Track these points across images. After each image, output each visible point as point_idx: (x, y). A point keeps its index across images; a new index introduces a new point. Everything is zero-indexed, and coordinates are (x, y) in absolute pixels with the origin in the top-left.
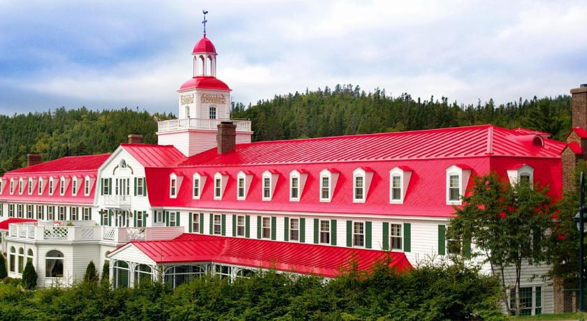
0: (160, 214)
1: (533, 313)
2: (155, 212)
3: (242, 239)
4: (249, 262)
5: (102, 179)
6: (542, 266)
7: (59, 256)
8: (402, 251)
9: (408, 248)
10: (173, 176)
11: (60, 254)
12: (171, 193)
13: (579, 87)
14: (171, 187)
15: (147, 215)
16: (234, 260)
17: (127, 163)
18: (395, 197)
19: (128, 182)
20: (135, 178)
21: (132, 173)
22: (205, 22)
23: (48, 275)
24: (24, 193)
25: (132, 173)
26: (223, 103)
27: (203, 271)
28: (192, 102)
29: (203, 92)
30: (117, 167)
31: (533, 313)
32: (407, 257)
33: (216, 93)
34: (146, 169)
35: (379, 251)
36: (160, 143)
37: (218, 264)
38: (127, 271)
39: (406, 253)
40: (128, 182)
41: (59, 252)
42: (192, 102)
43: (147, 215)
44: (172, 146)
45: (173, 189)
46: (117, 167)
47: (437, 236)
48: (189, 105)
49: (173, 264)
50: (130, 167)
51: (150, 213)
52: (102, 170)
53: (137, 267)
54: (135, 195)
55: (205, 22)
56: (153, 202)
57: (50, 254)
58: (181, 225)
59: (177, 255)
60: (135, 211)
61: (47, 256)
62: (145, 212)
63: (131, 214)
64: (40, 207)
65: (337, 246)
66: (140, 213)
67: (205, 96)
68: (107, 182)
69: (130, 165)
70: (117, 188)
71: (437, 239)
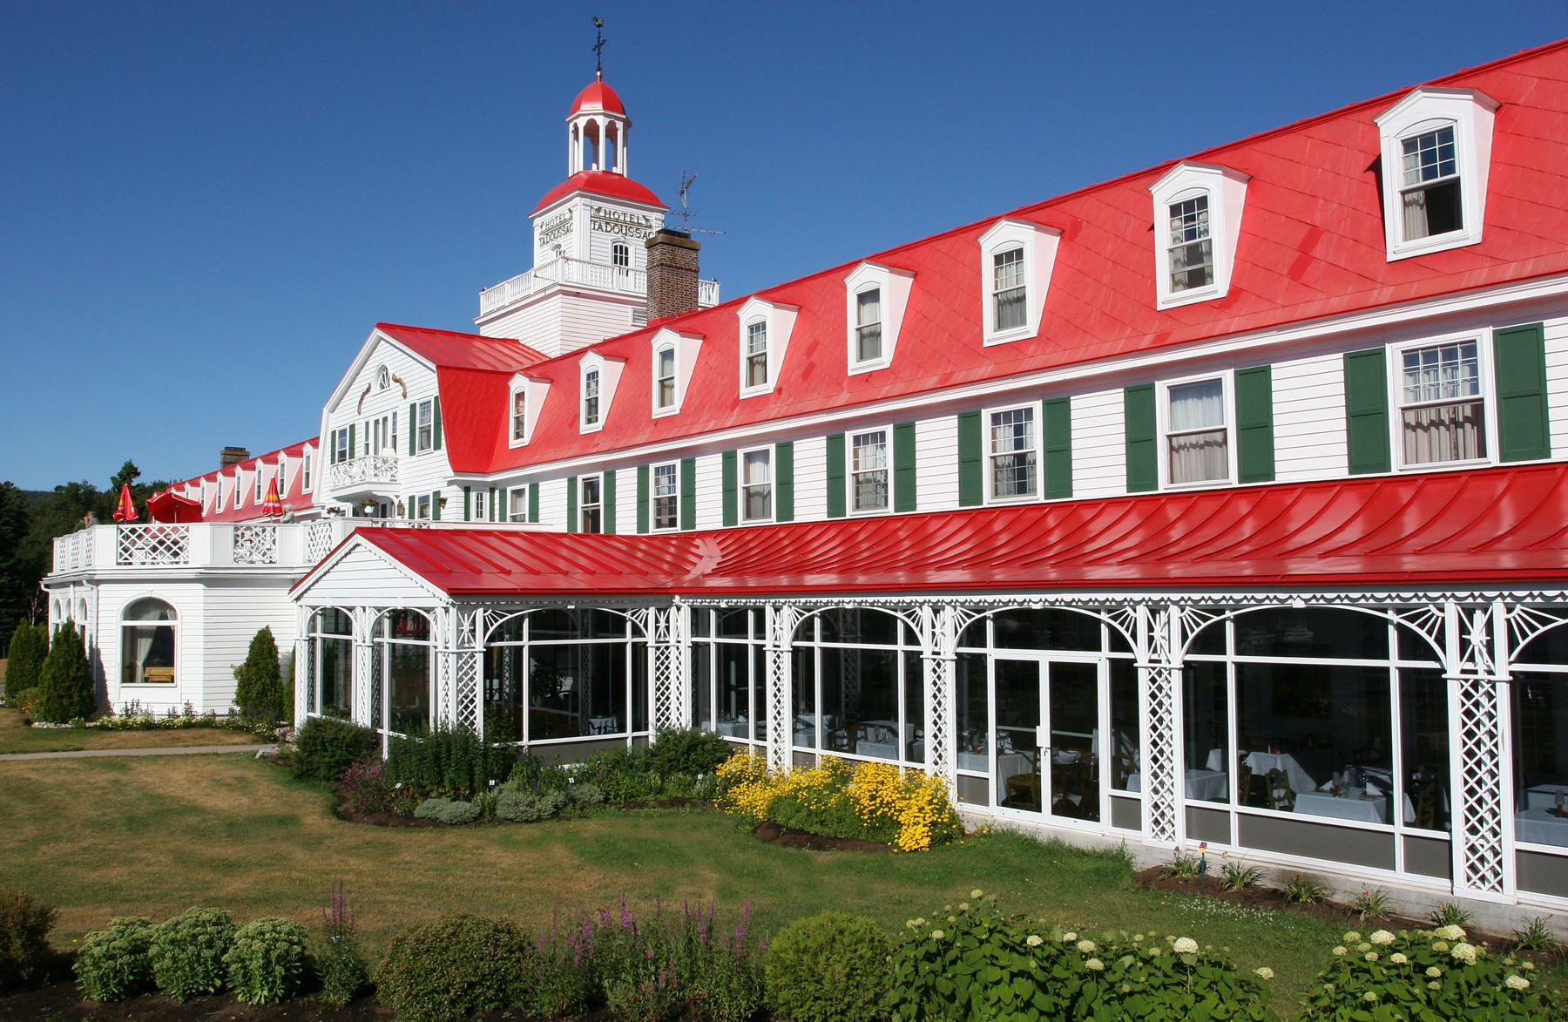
6: (229, 664)
7: (163, 617)
12: (571, 136)
14: (512, 414)
15: (444, 501)
19: (394, 423)
20: (413, 407)
21: (405, 396)
22: (598, 46)
23: (129, 675)
25: (405, 396)
27: (637, 631)
29: (597, 204)
37: (698, 602)
38: (426, 648)
40: (394, 423)
43: (444, 501)
44: (515, 342)
45: (519, 423)
46: (368, 390)
48: (561, 241)
50: (397, 381)
54: (412, 452)
55: (598, 46)
56: (458, 464)
57: (138, 609)
59: (538, 573)
62: (437, 494)
63: (401, 506)
66: (424, 500)
67: (602, 214)
69: (398, 376)
70: (367, 445)
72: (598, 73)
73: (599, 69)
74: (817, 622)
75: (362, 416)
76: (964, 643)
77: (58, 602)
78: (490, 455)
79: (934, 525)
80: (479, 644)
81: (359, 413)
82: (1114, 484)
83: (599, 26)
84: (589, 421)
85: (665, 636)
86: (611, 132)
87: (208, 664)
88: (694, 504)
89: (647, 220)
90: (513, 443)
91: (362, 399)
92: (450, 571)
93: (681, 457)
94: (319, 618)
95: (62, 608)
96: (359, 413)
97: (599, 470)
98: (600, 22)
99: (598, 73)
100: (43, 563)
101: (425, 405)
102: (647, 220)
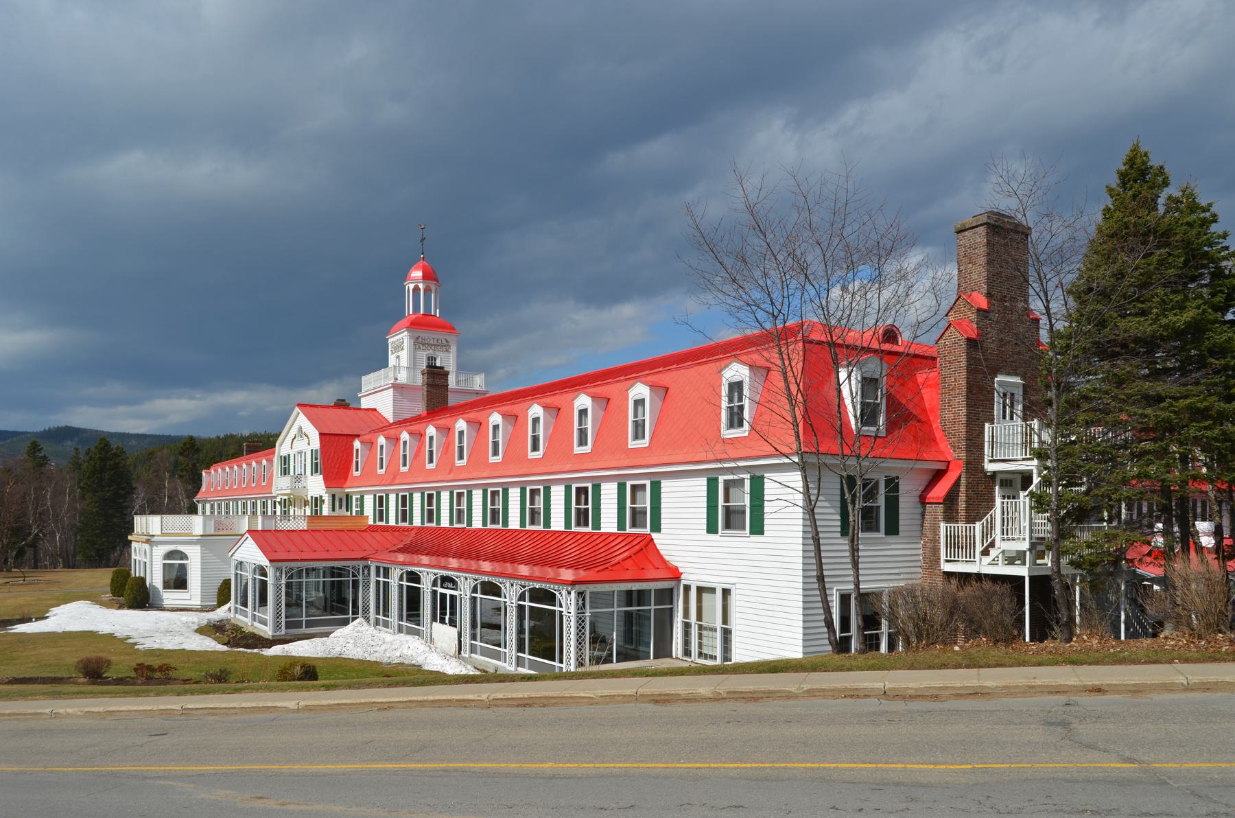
0: (341, 500)
1: (884, 647)
2: (334, 496)
3: (405, 527)
4: (550, 572)
5: (281, 456)
7: (182, 559)
8: (647, 531)
9: (656, 527)
10: (357, 444)
11: (183, 556)
13: (971, 219)
16: (425, 559)
17: (304, 430)
18: (636, 437)
20: (312, 450)
21: (309, 444)
22: (423, 240)
24: (238, 486)
25: (309, 444)
26: (447, 351)
28: (403, 349)
29: (417, 334)
30: (295, 437)
31: (884, 647)
32: (656, 541)
33: (436, 337)
34: (320, 434)
35: (611, 534)
36: (363, 407)
39: (654, 535)
41: (182, 552)
42: (403, 349)
44: (375, 410)
47: (705, 499)
48: (400, 354)
49: (299, 564)
51: (326, 497)
52: (281, 445)
53: (435, 581)
54: (312, 475)
55: (423, 240)
56: (328, 482)
57: (170, 555)
58: (365, 515)
60: (312, 497)
61: (165, 559)
64: (253, 502)
65: (552, 529)
67: (420, 340)
68: (285, 460)
71: (705, 505)
72: (422, 256)
73: (423, 254)
74: (479, 587)
75: (293, 450)
76: (554, 603)
77: (135, 548)
78: (346, 478)
79: (612, 538)
80: (283, 581)
81: (292, 448)
82: (309, 514)
83: (422, 229)
84: (636, 437)
85: (582, 609)
86: (427, 290)
87: (203, 594)
88: (660, 514)
89: (447, 341)
90: (356, 474)
91: (292, 442)
92: (627, 569)
93: (650, 479)
94: (257, 570)
95: (138, 551)
96: (292, 448)
97: (498, 487)
98: (423, 227)
99: (422, 256)
100: (130, 529)
101: (316, 451)
102: (447, 341)
